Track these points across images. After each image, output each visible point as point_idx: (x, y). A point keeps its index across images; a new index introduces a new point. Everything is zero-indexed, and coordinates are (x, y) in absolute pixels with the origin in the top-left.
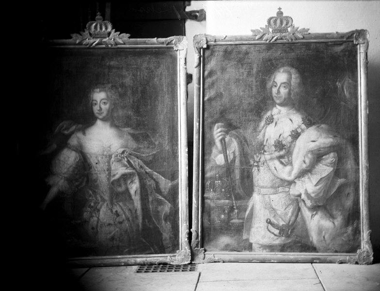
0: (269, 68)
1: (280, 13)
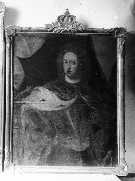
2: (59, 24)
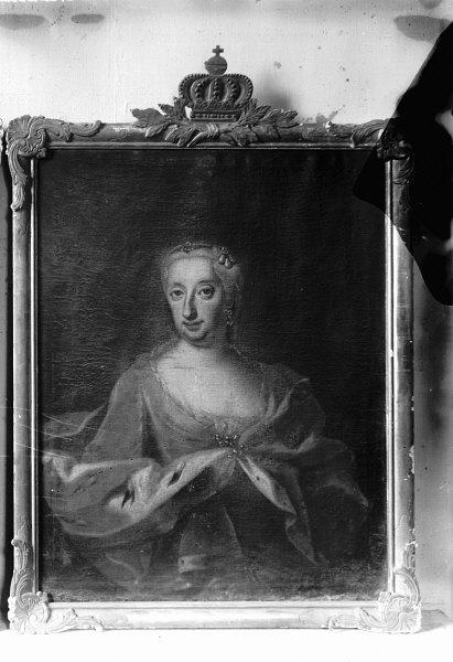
0: (158, 234)
1: (218, 64)
2: (188, 111)
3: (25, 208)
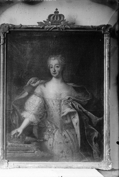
2: (50, 22)
3: (4, 44)
